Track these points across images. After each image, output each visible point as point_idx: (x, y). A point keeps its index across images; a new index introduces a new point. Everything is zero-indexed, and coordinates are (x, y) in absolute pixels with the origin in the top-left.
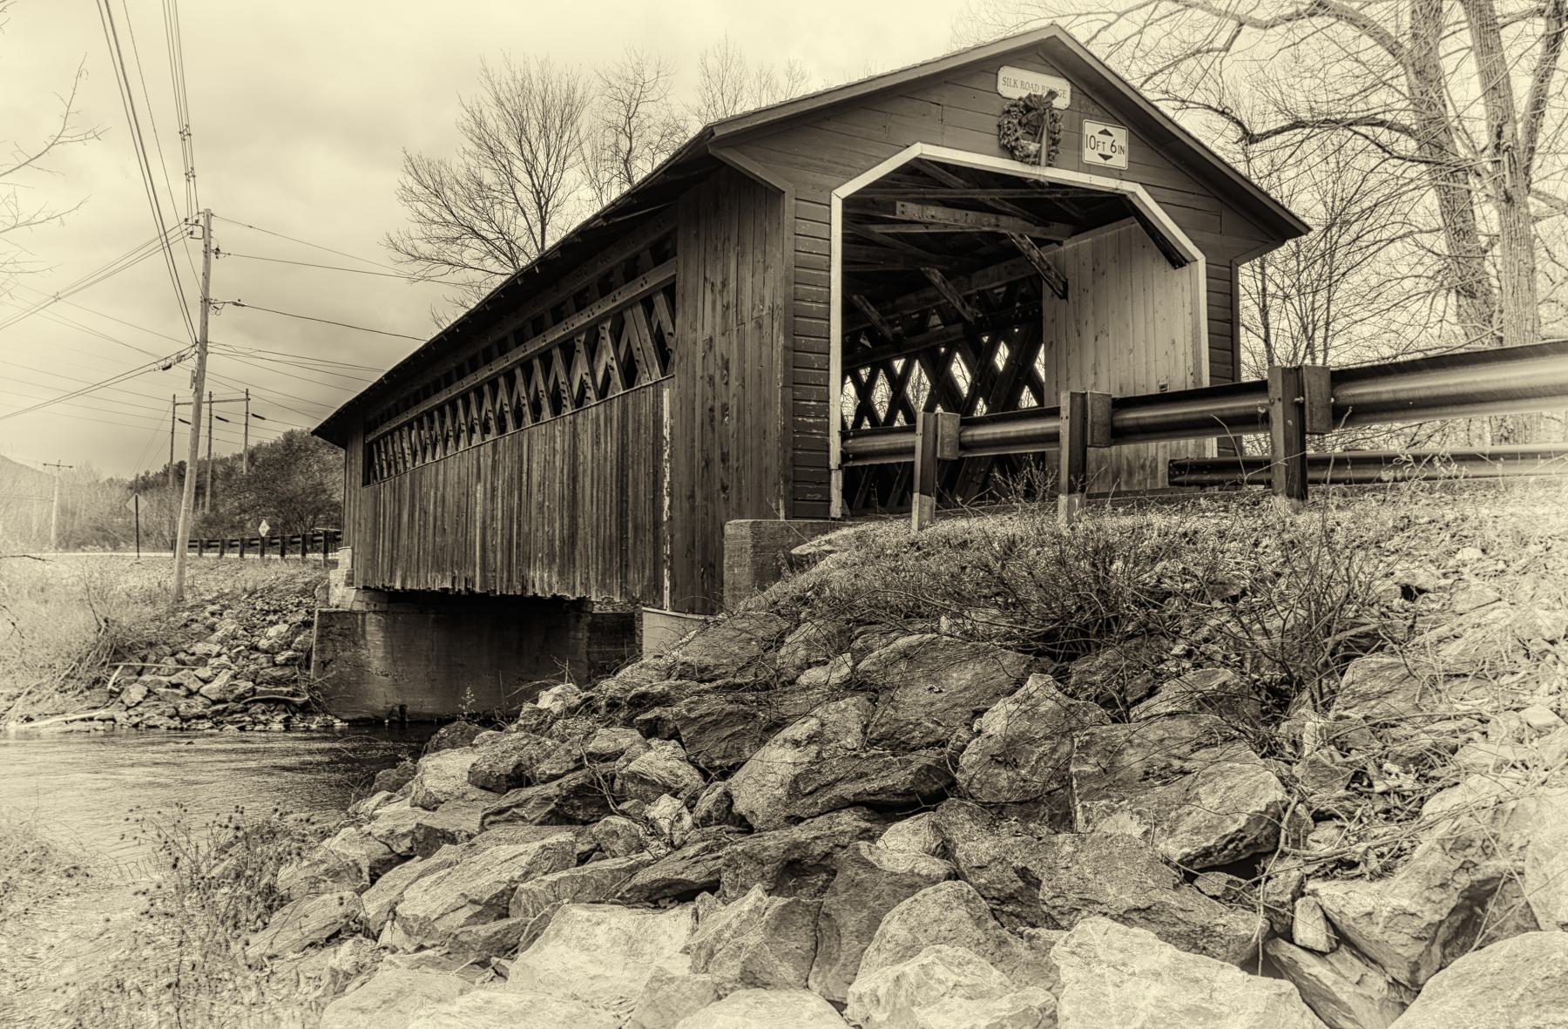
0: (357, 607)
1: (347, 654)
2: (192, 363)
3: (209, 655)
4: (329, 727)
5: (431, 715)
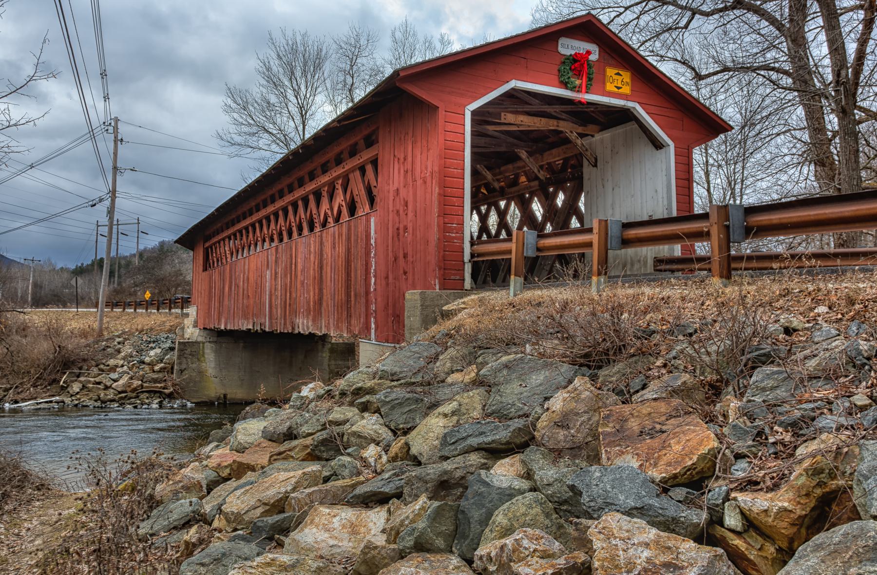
0: (200, 339)
1: (194, 365)
2: (107, 203)
3: (117, 366)
4: (184, 406)
5: (241, 400)
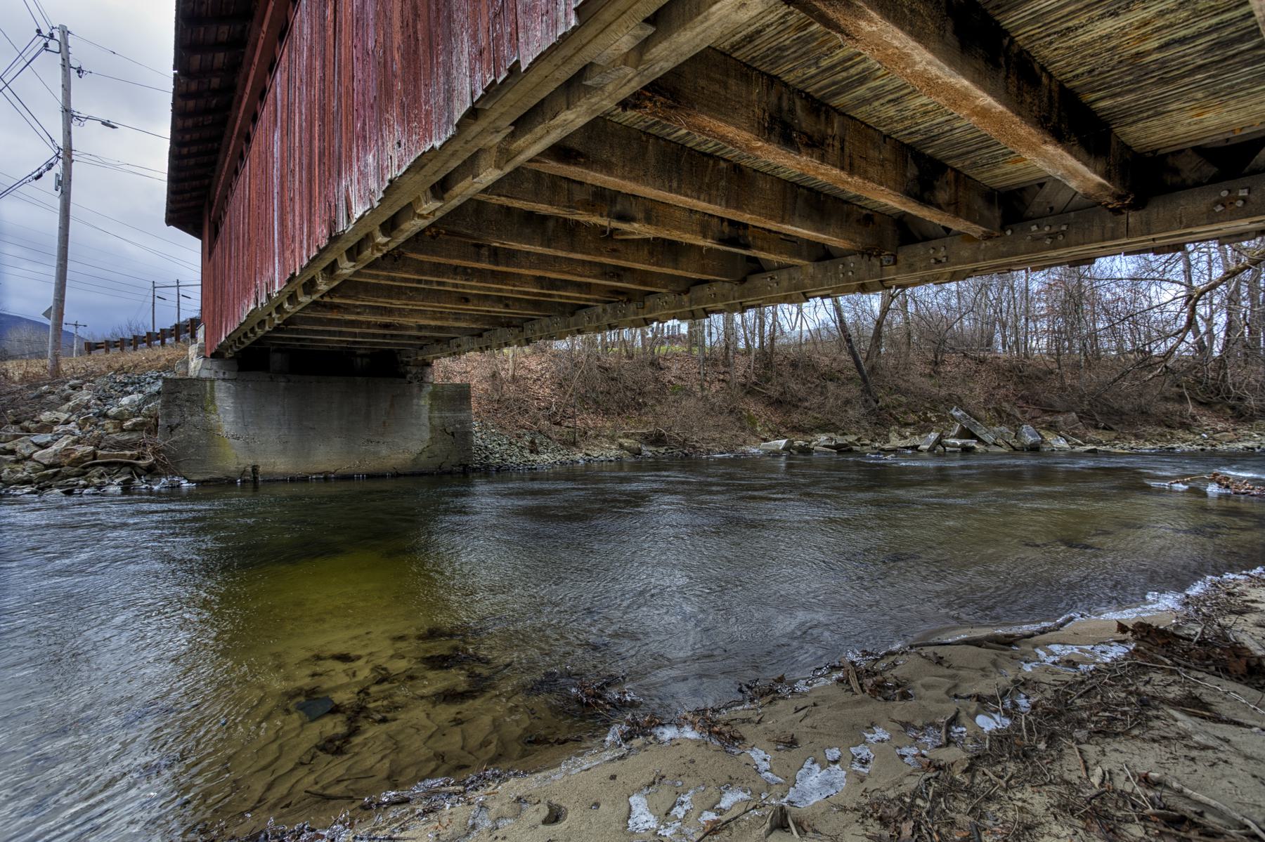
0: (205, 374)
1: (196, 418)
2: (58, 168)
3: (56, 423)
4: (175, 487)
5: (283, 474)
